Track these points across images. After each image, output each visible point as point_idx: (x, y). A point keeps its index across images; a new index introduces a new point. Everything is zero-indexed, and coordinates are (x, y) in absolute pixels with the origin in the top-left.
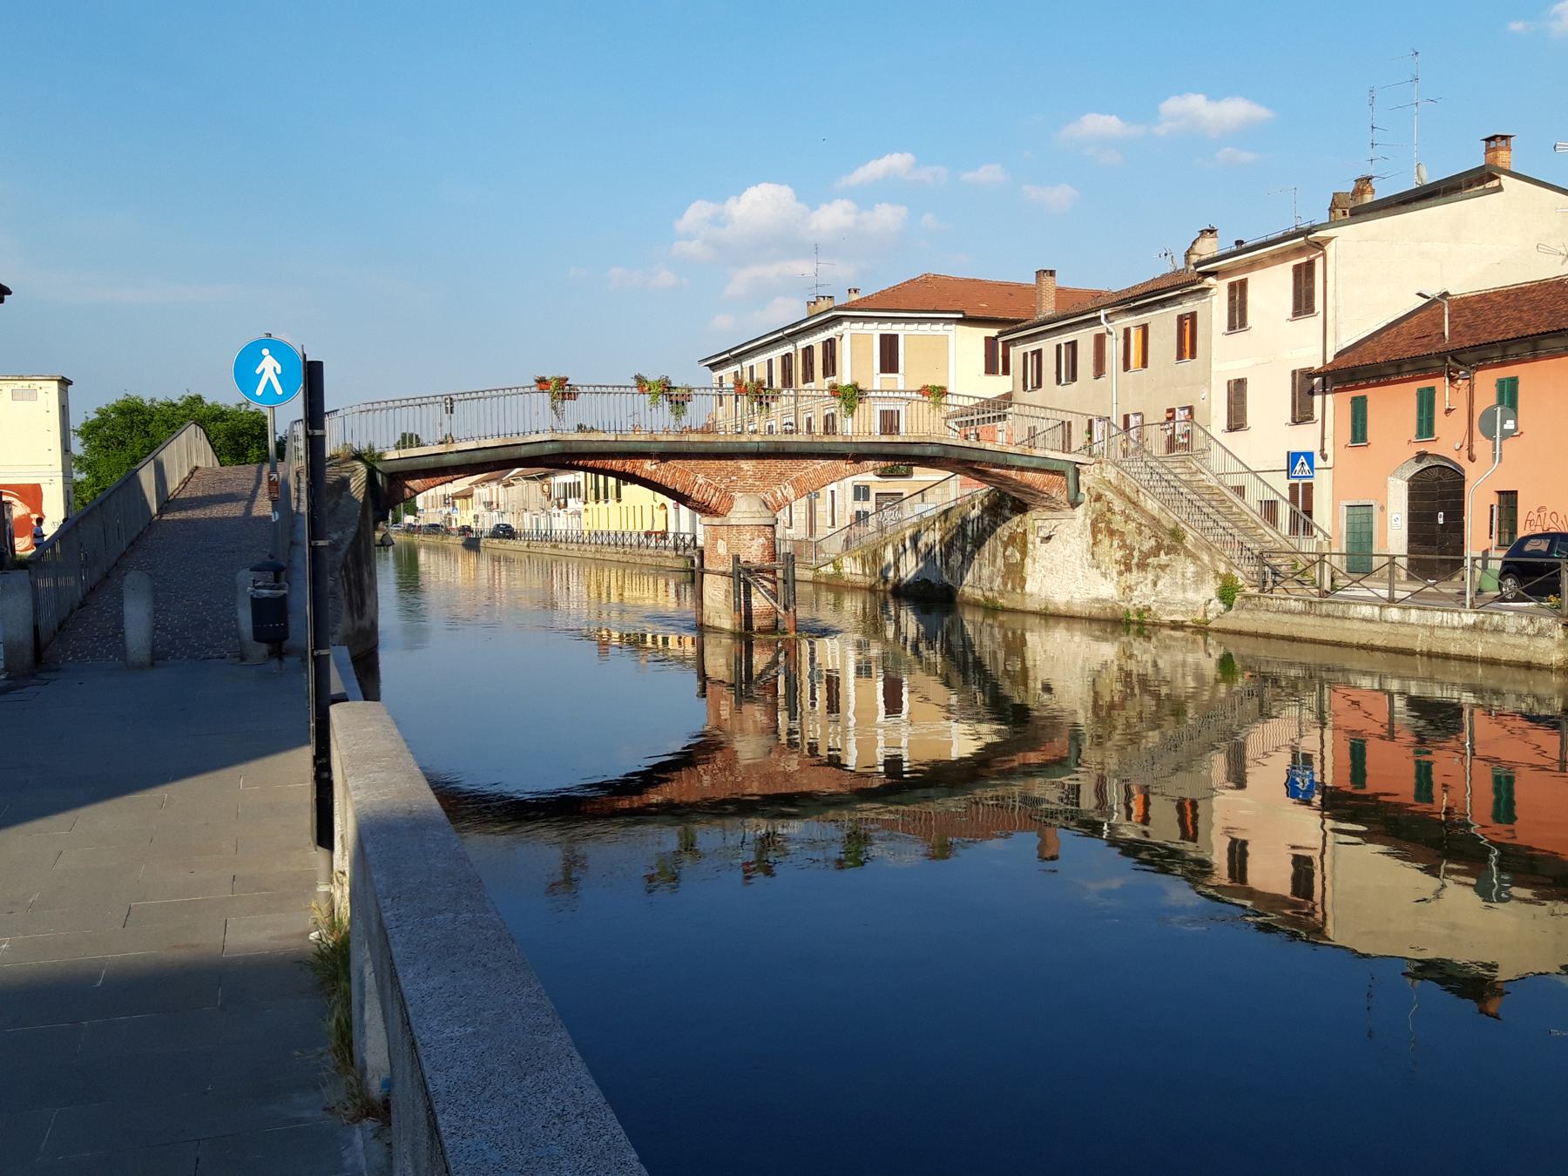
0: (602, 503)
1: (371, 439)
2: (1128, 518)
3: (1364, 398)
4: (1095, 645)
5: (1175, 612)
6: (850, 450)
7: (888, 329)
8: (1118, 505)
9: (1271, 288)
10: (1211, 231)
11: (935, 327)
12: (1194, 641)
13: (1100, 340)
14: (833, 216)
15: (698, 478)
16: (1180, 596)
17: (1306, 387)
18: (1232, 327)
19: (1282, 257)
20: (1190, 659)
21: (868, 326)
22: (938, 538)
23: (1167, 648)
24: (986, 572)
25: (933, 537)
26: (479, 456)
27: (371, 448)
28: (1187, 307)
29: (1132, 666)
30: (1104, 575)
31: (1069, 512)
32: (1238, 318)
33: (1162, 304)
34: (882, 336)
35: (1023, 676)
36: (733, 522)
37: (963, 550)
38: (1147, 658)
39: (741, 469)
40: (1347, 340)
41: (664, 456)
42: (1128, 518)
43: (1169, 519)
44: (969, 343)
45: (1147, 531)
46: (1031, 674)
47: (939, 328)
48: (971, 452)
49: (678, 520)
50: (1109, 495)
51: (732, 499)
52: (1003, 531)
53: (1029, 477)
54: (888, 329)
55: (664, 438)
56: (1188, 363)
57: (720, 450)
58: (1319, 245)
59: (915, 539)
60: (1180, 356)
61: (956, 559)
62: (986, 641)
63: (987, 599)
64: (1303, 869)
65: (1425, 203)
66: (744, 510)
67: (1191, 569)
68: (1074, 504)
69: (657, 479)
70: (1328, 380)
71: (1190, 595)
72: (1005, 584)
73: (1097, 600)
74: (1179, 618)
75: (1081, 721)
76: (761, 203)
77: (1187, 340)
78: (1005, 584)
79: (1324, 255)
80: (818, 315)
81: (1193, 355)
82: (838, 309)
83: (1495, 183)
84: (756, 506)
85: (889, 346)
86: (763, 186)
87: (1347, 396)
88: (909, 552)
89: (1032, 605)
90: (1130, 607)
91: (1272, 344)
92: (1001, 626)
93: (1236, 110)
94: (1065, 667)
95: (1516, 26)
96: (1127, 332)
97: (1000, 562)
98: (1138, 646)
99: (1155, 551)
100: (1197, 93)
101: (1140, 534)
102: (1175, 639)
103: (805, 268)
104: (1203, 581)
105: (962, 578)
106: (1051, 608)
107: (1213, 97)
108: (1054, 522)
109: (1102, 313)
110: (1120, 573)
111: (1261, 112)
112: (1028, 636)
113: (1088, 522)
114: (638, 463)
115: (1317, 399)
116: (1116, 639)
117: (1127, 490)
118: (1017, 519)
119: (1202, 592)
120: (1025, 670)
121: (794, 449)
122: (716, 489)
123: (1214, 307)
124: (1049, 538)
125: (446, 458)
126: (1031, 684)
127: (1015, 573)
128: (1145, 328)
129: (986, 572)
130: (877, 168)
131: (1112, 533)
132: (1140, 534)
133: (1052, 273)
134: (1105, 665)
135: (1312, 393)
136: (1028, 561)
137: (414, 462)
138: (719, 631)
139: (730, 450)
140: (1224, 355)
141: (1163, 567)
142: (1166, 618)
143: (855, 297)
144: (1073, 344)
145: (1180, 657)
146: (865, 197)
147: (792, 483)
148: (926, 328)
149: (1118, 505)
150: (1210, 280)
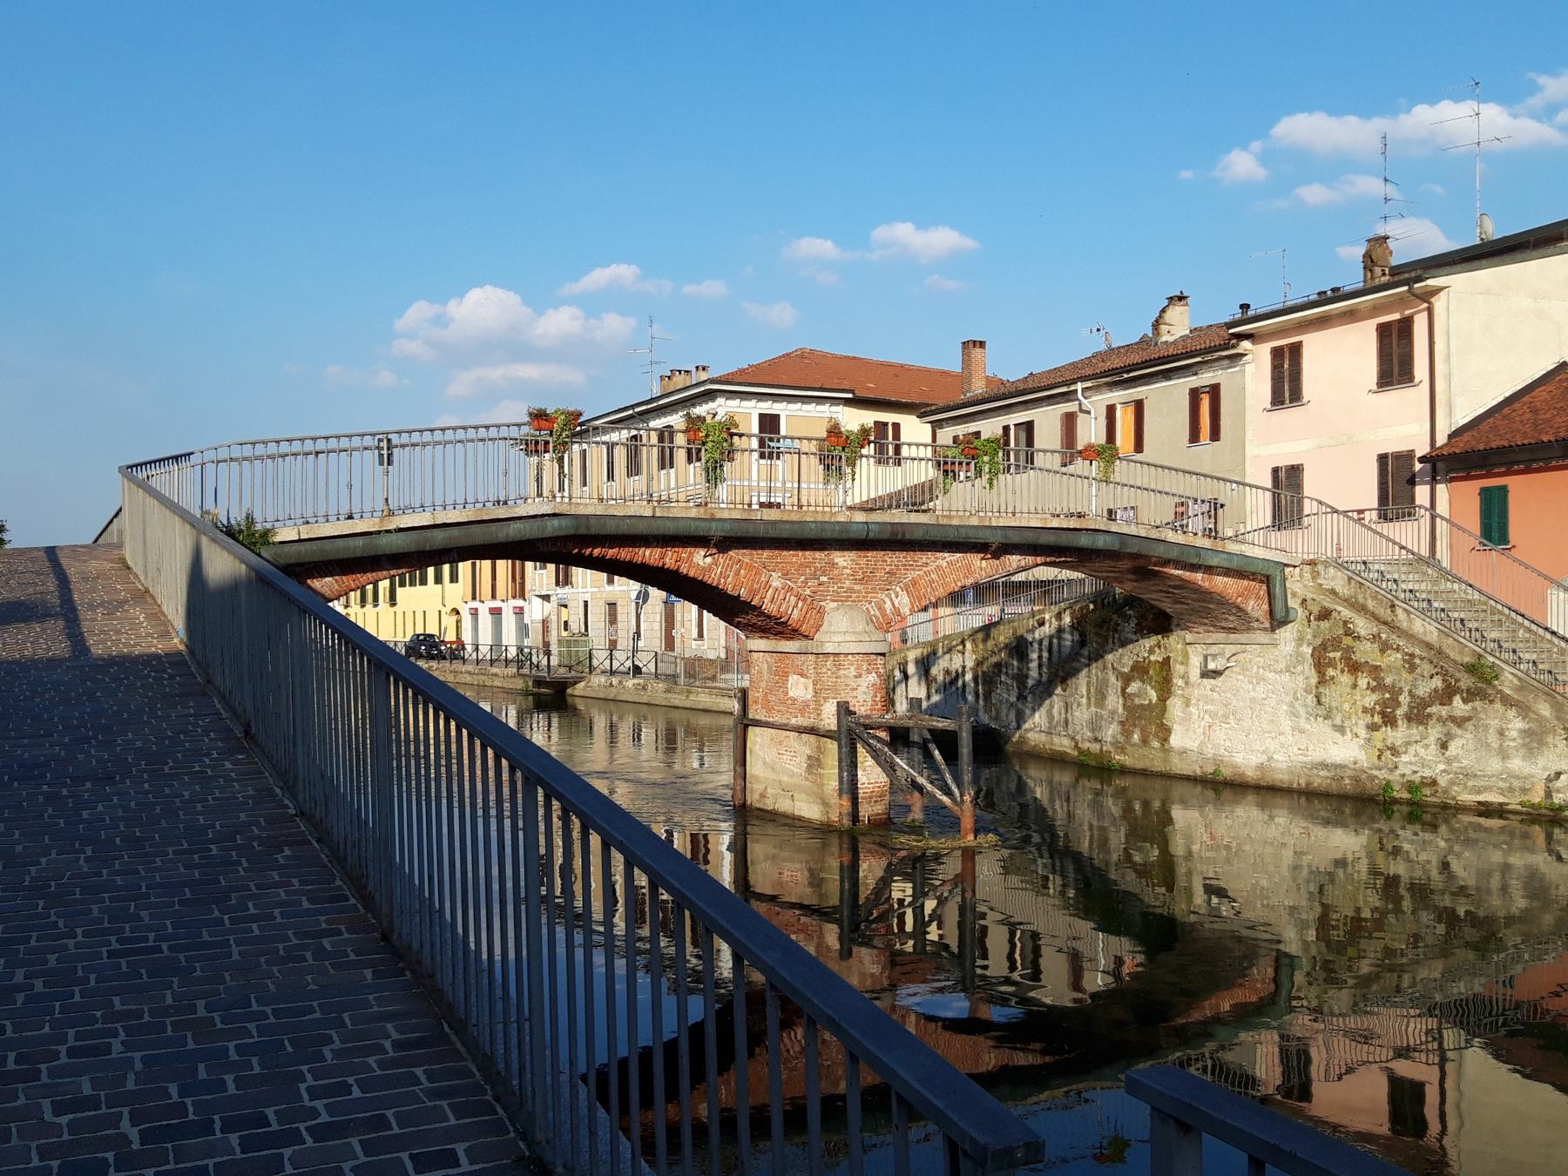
0: (369, 607)
1: (246, 505)
2: (1385, 647)
3: (1503, 490)
4: (1318, 832)
5: (1486, 789)
6: (996, 539)
7: (768, 407)
8: (1362, 626)
9: (1341, 357)
10: (1181, 298)
11: (820, 408)
12: (1525, 836)
13: (1069, 421)
14: (561, 322)
15: (768, 580)
16: (1495, 764)
17: (1397, 480)
18: (1278, 401)
19: (1376, 310)
20: (1516, 860)
21: (745, 404)
22: (970, 664)
23: (1468, 842)
24: (1081, 715)
25: (964, 661)
26: (439, 538)
27: (250, 520)
28: (1206, 378)
29: (1398, 868)
30: (1341, 729)
31: (1262, 637)
32: (1287, 385)
33: (1167, 375)
34: (761, 415)
35: (1166, 870)
36: (829, 648)
37: (1021, 678)
38: (1430, 857)
39: (833, 565)
40: (1463, 417)
41: (726, 543)
42: (1385, 647)
43: (1460, 651)
45: (1426, 668)
46: (1181, 870)
48: (1154, 545)
49: (475, 628)
50: (1346, 613)
51: (821, 612)
52: (1123, 658)
53: (1220, 583)
54: (768, 407)
55: (726, 515)
56: (1206, 448)
57: (812, 535)
58: (1428, 296)
59: (925, 665)
60: (1194, 437)
61: (1006, 693)
62: (1084, 813)
63: (1088, 753)
64: (1406, 1100)
65: (1496, 259)
66: (842, 629)
67: (1517, 725)
68: (1277, 620)
69: (712, 578)
70: (1440, 465)
71: (1517, 764)
72: (1127, 734)
73: (1324, 765)
74: (1494, 798)
75: (1293, 948)
76: (483, 307)
77: (1207, 413)
78: (1127, 734)
79: (1430, 311)
80: (672, 393)
81: (1215, 435)
82: (713, 381)
84: (861, 626)
85: (769, 423)
86: (489, 289)
87: (1470, 490)
88: (913, 682)
89: (1179, 766)
90: (1394, 777)
91: (1345, 420)
92: (1120, 793)
93: (943, 239)
94: (1252, 866)
95: (1186, 174)
96: (1111, 410)
97: (1114, 701)
98: (1408, 839)
99: (1446, 695)
101: (1412, 668)
102: (1488, 830)
103: (528, 371)
104: (1542, 743)
105: (1020, 719)
106: (1226, 772)
107: (923, 225)
108: (1229, 650)
109: (1079, 386)
110: (1373, 727)
111: (968, 243)
112: (1177, 813)
113: (1307, 650)
114: (684, 553)
115: (1422, 493)
116: (1364, 825)
117: (1370, 604)
118: (1148, 643)
119: (1541, 762)
120: (1167, 865)
121: (918, 535)
122: (798, 597)
123: (1254, 371)
124: (1216, 674)
125: (384, 540)
126: (1181, 881)
127: (1150, 721)
128: (1139, 406)
129: (1081, 715)
130: (599, 277)
131: (1354, 668)
132: (1412, 668)
133: (982, 344)
134: (1341, 863)
135: (1412, 482)
136: (1175, 706)
137: (328, 545)
138: (792, 822)
139: (828, 535)
140: (1262, 438)
141: (1460, 722)
142: (1467, 798)
143: (704, 376)
144: (1029, 427)
145: (1496, 857)
146: (594, 305)
147: (906, 589)
149: (1362, 626)
150: (1246, 345)
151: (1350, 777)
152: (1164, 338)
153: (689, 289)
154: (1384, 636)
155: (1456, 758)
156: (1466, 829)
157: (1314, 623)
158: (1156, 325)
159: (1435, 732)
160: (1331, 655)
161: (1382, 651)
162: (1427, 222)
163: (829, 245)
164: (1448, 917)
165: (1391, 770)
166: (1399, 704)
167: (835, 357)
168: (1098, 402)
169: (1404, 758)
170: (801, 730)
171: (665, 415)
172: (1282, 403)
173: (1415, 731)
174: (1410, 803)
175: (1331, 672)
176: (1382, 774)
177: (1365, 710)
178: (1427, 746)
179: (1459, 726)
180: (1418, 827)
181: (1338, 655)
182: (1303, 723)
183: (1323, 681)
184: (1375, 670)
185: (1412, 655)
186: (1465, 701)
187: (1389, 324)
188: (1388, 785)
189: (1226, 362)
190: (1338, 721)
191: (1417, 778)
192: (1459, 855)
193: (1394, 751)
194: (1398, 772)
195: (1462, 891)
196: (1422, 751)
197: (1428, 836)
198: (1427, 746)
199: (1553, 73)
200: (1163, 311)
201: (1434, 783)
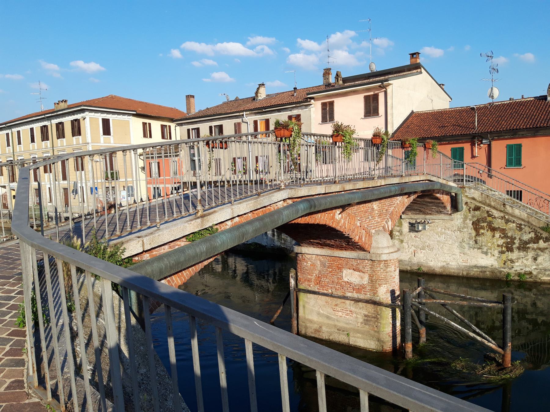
8: (496, 213)
30: (486, 253)
31: (446, 217)
38: (528, 301)
42: (507, 221)
44: (136, 124)
45: (527, 229)
47: (126, 117)
50: (487, 208)
73: (476, 266)
83: (419, 70)
85: (106, 123)
90: (512, 271)
93: (93, 67)
95: (161, 55)
99: (536, 240)
100: (80, 60)
101: (521, 229)
106: (425, 269)
109: (245, 113)
110: (502, 252)
111: (103, 69)
113: (469, 223)
131: (493, 230)
132: (521, 229)
133: (193, 97)
141: (542, 250)
148: (121, 117)
149: (496, 213)
150: (312, 101)
151: (489, 272)
152: (260, 98)
153: (8, 76)
154: (507, 217)
155: (541, 264)
156: (544, 290)
157: (472, 212)
158: (257, 93)
159: (531, 254)
160: (482, 224)
161: (506, 223)
162: (223, 73)
163: (56, 66)
164: (534, 322)
165: (510, 269)
166: (514, 243)
167: (123, 99)
168: (250, 119)
169: (517, 264)
170: (367, 302)
171: (59, 118)
172: (326, 121)
173: (522, 254)
174: (519, 281)
175: (482, 231)
176: (506, 270)
177: (498, 246)
178: (527, 260)
179: (542, 251)
180: (522, 290)
181: (485, 224)
182: (466, 250)
183: (478, 234)
184: (503, 231)
185: (521, 225)
186: (545, 242)
187: (369, 96)
188: (508, 274)
189: (304, 107)
190: (485, 250)
191: (523, 272)
192: (540, 300)
193: (512, 261)
194: (514, 269)
195: (542, 313)
196: (525, 262)
197: (527, 293)
198: (527, 260)
199: (252, 37)
200: (258, 89)
201: (531, 273)
